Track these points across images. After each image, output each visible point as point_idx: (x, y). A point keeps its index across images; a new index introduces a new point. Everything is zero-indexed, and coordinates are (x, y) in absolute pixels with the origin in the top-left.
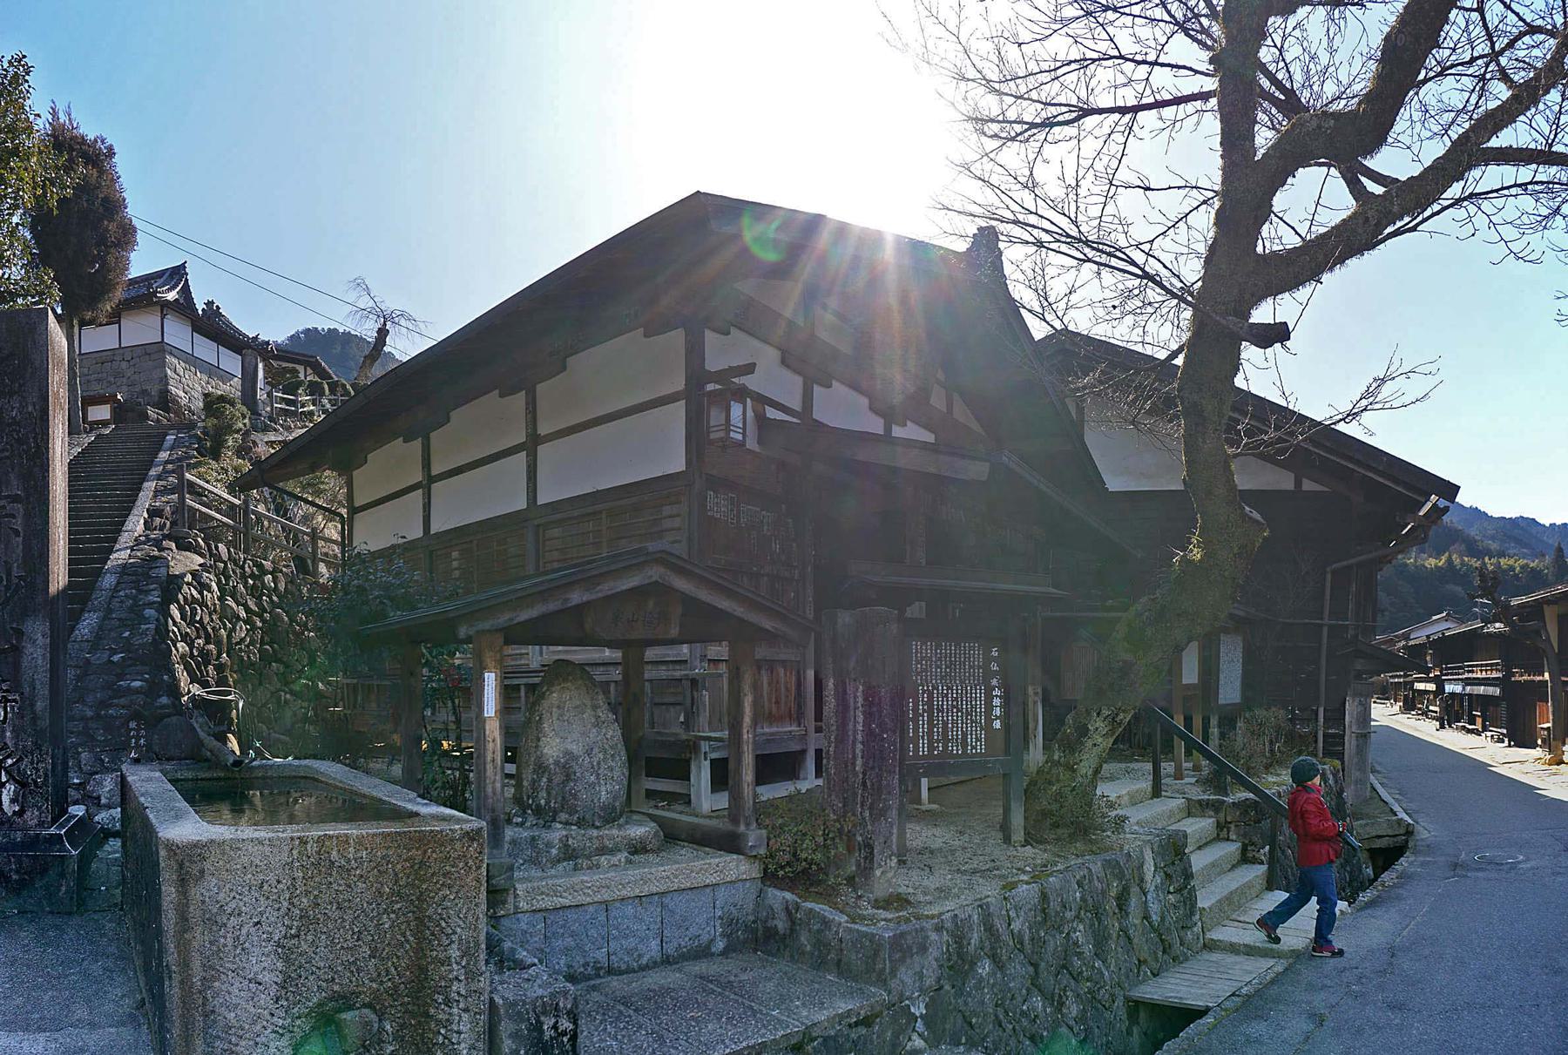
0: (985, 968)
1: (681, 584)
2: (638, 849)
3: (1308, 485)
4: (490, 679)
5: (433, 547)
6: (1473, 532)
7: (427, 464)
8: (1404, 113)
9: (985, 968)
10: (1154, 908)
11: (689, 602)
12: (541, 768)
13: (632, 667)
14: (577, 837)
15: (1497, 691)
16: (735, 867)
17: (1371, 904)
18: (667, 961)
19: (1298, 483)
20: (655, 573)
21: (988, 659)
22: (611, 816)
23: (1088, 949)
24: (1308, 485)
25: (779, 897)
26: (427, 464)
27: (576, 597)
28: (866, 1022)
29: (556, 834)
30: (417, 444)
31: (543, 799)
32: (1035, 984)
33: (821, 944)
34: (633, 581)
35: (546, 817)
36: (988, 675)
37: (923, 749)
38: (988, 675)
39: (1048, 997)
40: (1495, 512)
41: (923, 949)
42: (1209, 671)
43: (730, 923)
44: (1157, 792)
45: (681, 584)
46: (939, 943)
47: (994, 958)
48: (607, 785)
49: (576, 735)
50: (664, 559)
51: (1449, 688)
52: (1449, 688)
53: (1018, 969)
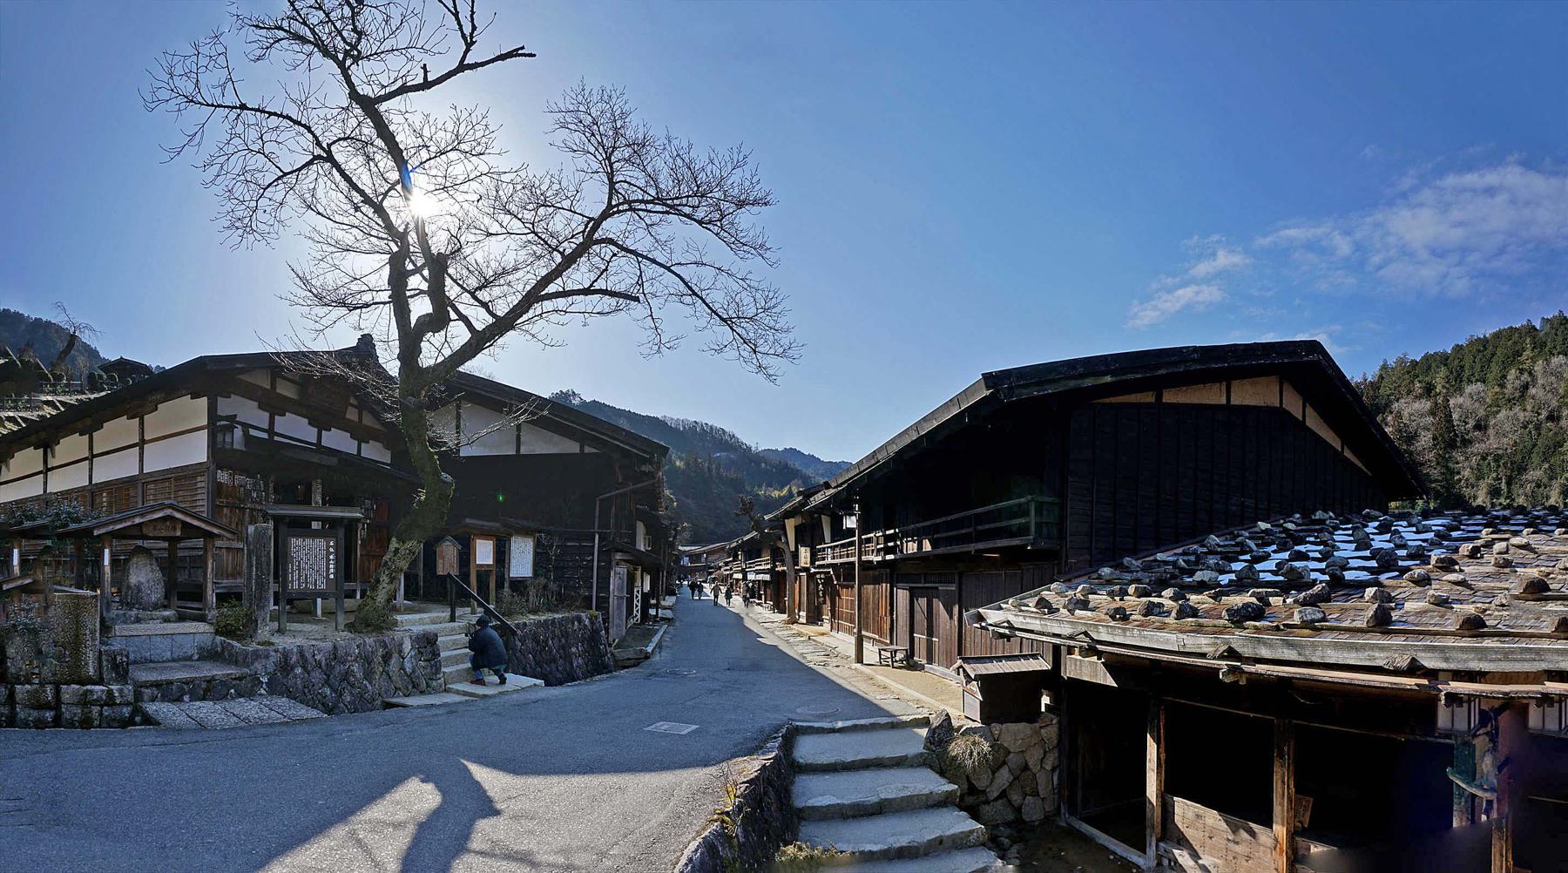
0: (299, 671)
1: (178, 515)
2: (167, 620)
3: (587, 450)
4: (107, 551)
5: (92, 492)
6: (809, 472)
7: (91, 448)
8: (379, 352)
9: (299, 671)
10: (408, 667)
11: (184, 524)
12: (129, 587)
13: (172, 549)
14: (142, 614)
15: (767, 577)
16: (202, 627)
17: (781, 727)
18: (174, 660)
19: (582, 448)
20: (169, 512)
21: (328, 547)
22: (156, 607)
23: (359, 675)
24: (587, 450)
25: (219, 638)
26: (91, 448)
27: (138, 520)
28: (240, 679)
29: (134, 612)
30: (86, 437)
31: (131, 599)
32: (327, 682)
33: (231, 655)
34: (160, 515)
35: (130, 606)
36: (329, 554)
37: (296, 586)
38: (329, 554)
39: (333, 690)
40: (825, 457)
41: (267, 657)
42: (502, 555)
43: (201, 648)
44: (453, 619)
45: (178, 515)
46: (274, 657)
47: (304, 667)
48: (156, 595)
49: (143, 575)
50: (171, 506)
51: (751, 577)
52: (751, 577)
53: (317, 676)
